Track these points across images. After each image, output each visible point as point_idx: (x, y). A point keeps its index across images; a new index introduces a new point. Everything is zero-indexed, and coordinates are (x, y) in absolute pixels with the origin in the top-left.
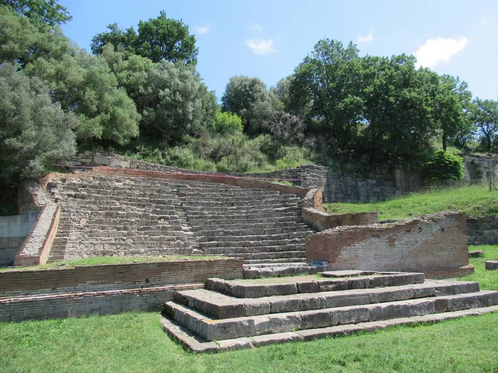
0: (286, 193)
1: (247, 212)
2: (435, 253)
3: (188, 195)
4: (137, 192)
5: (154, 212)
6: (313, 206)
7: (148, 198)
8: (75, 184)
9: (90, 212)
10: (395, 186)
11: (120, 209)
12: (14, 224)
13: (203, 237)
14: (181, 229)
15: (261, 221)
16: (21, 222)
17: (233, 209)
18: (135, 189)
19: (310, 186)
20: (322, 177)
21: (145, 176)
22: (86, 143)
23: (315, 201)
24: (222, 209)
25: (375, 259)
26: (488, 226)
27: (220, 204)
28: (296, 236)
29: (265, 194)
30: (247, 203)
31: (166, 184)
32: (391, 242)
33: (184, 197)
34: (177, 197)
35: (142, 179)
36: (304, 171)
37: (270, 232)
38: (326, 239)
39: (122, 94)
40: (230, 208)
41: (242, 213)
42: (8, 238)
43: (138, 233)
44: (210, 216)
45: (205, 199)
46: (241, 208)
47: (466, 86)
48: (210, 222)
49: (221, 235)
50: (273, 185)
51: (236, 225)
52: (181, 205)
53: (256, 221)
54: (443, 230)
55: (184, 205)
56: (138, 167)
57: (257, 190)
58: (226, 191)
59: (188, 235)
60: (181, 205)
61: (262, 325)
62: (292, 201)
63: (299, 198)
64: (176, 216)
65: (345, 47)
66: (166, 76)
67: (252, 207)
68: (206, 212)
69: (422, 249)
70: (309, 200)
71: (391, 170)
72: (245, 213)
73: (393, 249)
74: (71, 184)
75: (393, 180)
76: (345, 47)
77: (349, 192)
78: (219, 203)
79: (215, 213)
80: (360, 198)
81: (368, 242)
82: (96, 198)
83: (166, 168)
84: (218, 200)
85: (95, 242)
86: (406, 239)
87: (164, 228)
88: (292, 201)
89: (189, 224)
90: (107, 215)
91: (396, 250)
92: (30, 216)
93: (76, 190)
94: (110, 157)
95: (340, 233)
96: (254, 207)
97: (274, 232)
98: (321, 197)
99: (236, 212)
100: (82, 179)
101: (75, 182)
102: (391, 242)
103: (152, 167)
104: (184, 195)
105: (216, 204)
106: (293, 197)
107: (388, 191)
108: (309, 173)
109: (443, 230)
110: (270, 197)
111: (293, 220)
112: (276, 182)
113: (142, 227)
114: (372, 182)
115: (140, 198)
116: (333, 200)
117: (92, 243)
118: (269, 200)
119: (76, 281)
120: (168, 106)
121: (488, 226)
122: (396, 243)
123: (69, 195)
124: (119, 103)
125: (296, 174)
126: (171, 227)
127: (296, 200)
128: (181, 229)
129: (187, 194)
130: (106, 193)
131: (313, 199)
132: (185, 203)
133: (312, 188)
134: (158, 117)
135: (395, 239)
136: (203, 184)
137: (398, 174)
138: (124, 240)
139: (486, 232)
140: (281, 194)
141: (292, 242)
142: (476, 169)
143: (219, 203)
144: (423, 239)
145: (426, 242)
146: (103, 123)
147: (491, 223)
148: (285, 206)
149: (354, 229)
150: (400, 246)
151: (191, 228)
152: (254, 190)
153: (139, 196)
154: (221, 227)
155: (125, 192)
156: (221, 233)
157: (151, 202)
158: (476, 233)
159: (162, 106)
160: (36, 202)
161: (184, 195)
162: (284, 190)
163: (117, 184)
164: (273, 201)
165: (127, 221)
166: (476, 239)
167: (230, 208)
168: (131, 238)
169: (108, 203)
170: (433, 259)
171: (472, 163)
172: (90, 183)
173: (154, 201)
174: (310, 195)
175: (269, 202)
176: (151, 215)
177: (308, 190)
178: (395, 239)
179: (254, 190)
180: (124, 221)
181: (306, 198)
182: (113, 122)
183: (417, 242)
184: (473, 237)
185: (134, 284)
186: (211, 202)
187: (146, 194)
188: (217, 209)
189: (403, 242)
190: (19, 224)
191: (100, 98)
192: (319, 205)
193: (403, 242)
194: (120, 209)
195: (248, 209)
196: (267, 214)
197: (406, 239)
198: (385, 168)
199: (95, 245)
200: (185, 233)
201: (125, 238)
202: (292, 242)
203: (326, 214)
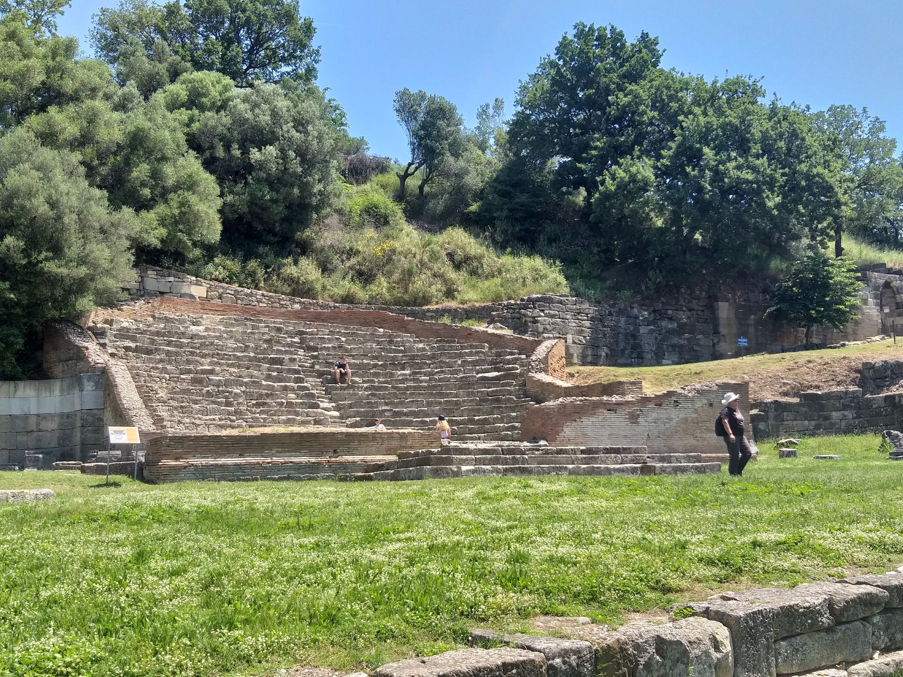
0: (500, 347)
1: (430, 380)
2: (698, 435)
3: (321, 349)
4: (231, 344)
5: (269, 377)
6: (546, 371)
7: (252, 355)
8: (128, 330)
9: (167, 376)
10: (716, 332)
11: (211, 372)
12: (48, 394)
13: (358, 419)
14: (318, 407)
15: (456, 396)
16: (62, 391)
17: (405, 375)
18: (226, 339)
19: (545, 335)
20: (568, 317)
21: (238, 313)
22: (146, 256)
23: (550, 361)
24: (385, 376)
25: (609, 438)
26: (838, 405)
27: (381, 365)
28: (514, 419)
29: (462, 348)
30: (430, 364)
31: (279, 330)
32: (633, 418)
33: (316, 353)
34: (301, 352)
35: (235, 319)
36: (535, 308)
37: (473, 414)
38: (547, 414)
39: (192, 164)
40: (399, 373)
41: (421, 382)
42: (38, 415)
43: (251, 412)
44: (365, 385)
45: (353, 356)
46: (420, 373)
47: (882, 129)
48: (368, 395)
49: (388, 417)
50: (476, 331)
51: (412, 401)
52: (313, 367)
53: (447, 395)
54: (711, 405)
55: (317, 367)
56: (220, 297)
57: (447, 342)
58: (391, 342)
59: (331, 417)
60: (313, 367)
61: (467, 471)
62: (509, 362)
63: (524, 357)
64: (306, 384)
65: (631, 39)
66: (265, 119)
67: (437, 372)
68: (357, 379)
69: (678, 429)
70: (540, 361)
71: (712, 300)
72: (425, 381)
73: (634, 426)
74: (122, 329)
75: (714, 321)
76: (631, 39)
77: (622, 345)
78: (380, 363)
79: (373, 382)
80: (645, 355)
81: (601, 417)
82: (168, 353)
83: (271, 297)
84: (376, 358)
85: (198, 422)
86: (655, 415)
87: (290, 404)
88: (509, 362)
89: (330, 399)
90: (194, 381)
91: (638, 429)
92: (85, 381)
93: (134, 339)
94: (172, 279)
95: (563, 405)
96: (442, 372)
97: (478, 412)
98: (564, 355)
99: (411, 380)
100: (136, 320)
101: (125, 324)
102: (633, 418)
103: (247, 295)
104: (315, 349)
105: (375, 366)
106: (512, 354)
107: (702, 343)
108: (543, 311)
109: (711, 405)
110: (471, 354)
111: (510, 393)
112: (482, 327)
113: (254, 402)
114: (670, 326)
115: (238, 354)
116: (589, 359)
117: (193, 423)
118: (469, 359)
119: (263, 447)
120: (275, 183)
121: (838, 405)
122: (640, 420)
123: (127, 349)
124: (190, 185)
125: (519, 313)
126: (301, 403)
127: (517, 359)
128: (318, 407)
129: (319, 346)
130: (181, 346)
131: (546, 358)
132: (318, 363)
133: (549, 338)
134: (253, 202)
135: (638, 415)
136: (346, 329)
137: (724, 310)
138: (231, 421)
139: (835, 415)
140: (490, 348)
141: (508, 429)
142: (894, 297)
143: (380, 363)
144: (680, 416)
145: (685, 420)
146: (162, 222)
147: (842, 401)
148: (496, 370)
149: (581, 401)
150: (646, 424)
151: (334, 404)
152: (440, 341)
153: (235, 350)
154: (386, 404)
155: (212, 344)
156: (387, 414)
157: (259, 360)
158: (819, 417)
159: (258, 181)
160: (90, 360)
161: (315, 349)
162: (496, 341)
163: (194, 328)
164: (477, 361)
165: (228, 392)
166: (818, 427)
167: (399, 373)
168: (243, 419)
169: (188, 362)
170: (695, 443)
171: (887, 285)
172: (149, 326)
173: (264, 359)
174: (541, 351)
175: (470, 362)
176: (264, 383)
177: (539, 343)
178: (638, 415)
179: (440, 341)
180: (224, 392)
181: (534, 358)
182: (185, 220)
183: (671, 420)
184: (813, 423)
185: (321, 454)
186: (365, 361)
187: (247, 346)
188: (376, 375)
189: (650, 419)
190: (57, 393)
191: (155, 175)
192: (557, 368)
193: (650, 419)
194: (211, 372)
195: (430, 374)
196: (466, 384)
197: (655, 415)
198: (698, 299)
199: (197, 425)
200: (326, 412)
201: (234, 418)
202: (508, 429)
203: (733, 382)
